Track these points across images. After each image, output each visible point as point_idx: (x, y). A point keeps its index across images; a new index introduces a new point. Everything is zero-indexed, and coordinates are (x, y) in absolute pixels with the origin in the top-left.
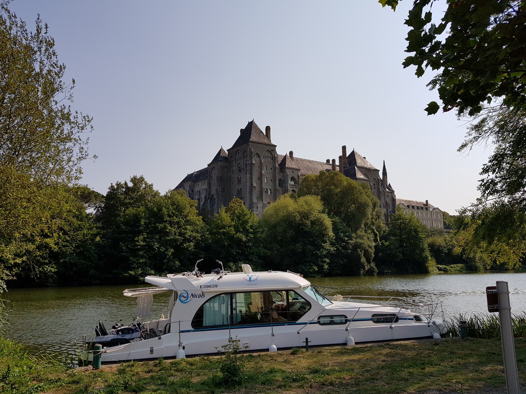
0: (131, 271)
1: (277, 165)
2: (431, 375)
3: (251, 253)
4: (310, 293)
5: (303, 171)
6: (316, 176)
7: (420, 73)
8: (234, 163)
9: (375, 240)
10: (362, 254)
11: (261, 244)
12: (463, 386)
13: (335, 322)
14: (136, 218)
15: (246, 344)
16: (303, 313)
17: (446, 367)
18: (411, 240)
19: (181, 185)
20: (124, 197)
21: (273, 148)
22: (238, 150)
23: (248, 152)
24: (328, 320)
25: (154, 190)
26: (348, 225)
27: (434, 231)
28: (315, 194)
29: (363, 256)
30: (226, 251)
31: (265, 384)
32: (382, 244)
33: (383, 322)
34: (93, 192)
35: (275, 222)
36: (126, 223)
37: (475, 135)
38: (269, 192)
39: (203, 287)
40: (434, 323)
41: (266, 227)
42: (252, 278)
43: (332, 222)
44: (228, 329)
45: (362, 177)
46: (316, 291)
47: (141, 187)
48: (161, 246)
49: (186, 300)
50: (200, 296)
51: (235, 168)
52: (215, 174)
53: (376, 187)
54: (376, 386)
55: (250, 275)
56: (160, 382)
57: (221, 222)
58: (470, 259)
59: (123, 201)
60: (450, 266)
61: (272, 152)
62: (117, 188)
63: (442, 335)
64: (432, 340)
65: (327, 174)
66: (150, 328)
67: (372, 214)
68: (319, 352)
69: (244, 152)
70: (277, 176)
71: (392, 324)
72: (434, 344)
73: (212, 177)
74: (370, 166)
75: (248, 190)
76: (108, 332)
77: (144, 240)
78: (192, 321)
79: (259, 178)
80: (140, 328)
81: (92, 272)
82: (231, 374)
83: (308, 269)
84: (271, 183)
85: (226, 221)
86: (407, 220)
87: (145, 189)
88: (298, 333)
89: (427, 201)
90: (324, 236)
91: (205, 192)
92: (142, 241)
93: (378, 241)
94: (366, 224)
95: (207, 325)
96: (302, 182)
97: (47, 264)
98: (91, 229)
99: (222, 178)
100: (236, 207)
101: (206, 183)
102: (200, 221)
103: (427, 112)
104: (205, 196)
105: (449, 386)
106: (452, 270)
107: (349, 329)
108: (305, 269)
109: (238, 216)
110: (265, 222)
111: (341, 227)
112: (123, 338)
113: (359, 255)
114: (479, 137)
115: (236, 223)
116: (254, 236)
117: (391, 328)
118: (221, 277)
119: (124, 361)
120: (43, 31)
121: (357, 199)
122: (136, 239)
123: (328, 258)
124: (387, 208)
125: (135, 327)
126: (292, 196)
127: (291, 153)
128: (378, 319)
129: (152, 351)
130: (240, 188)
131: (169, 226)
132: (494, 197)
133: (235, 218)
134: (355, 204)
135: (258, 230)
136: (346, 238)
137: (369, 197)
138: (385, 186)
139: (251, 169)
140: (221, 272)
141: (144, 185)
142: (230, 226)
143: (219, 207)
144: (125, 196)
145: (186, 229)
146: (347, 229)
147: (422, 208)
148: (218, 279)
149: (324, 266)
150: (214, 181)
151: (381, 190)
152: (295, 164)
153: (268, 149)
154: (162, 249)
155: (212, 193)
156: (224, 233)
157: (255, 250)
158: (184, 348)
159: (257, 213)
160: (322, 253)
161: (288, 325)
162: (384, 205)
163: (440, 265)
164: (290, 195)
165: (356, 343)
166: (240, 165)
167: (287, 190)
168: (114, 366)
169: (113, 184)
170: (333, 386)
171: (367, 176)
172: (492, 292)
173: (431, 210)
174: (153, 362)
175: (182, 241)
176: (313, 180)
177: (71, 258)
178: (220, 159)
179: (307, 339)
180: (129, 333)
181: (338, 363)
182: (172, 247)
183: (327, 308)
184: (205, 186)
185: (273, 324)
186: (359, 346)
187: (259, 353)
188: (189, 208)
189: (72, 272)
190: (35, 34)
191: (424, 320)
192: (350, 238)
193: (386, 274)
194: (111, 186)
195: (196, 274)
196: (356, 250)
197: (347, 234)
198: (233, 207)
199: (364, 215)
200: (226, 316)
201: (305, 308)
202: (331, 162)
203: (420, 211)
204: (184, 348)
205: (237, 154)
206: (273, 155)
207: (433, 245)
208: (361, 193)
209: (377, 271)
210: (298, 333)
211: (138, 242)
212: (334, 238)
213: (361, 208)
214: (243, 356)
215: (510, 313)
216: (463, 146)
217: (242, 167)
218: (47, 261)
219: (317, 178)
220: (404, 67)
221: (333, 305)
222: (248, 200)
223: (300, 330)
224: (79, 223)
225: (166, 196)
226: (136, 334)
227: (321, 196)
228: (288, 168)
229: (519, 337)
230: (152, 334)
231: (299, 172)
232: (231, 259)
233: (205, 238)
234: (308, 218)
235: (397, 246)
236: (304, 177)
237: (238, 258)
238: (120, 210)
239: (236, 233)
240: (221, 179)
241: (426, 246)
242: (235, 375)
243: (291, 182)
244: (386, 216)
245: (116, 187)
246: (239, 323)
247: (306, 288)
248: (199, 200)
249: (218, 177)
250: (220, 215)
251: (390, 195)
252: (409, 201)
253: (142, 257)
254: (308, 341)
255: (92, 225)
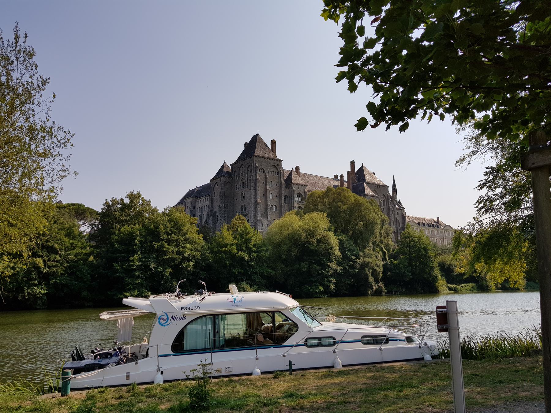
0: (126, 292)
1: (283, 181)
2: (406, 397)
3: (254, 272)
4: (298, 315)
5: (310, 187)
6: (322, 192)
7: (353, 88)
8: (238, 179)
9: (384, 259)
10: (370, 274)
11: (265, 264)
12: (434, 408)
13: (323, 343)
14: (131, 236)
15: (229, 368)
16: (290, 335)
17: (424, 389)
18: (421, 259)
19: (182, 202)
20: (119, 214)
21: (278, 163)
22: (242, 165)
23: (253, 167)
24: (316, 342)
25: (152, 207)
26: (356, 243)
27: (445, 249)
28: (321, 211)
29: (370, 275)
30: (227, 271)
31: (234, 409)
32: (391, 262)
33: (373, 344)
34: (88, 208)
35: (279, 241)
36: (121, 242)
37: (473, 149)
38: (274, 208)
39: (184, 309)
40: (426, 344)
41: (270, 245)
42: (237, 299)
43: (338, 241)
44: (210, 352)
45: (371, 193)
46: (305, 312)
47: (137, 203)
48: (158, 266)
49: (167, 322)
50: (181, 319)
51: (239, 184)
52: (218, 190)
53: (385, 204)
54: (347, 410)
55: (235, 296)
56: (126, 408)
57: (222, 240)
58: (481, 278)
59: (118, 218)
60: (461, 285)
61: (277, 167)
62: (113, 205)
63: (433, 357)
64: (422, 362)
65: (334, 190)
66: (131, 353)
67: (380, 233)
68: (302, 376)
69: (248, 167)
70: (283, 192)
71: (381, 346)
72: (422, 366)
73: (215, 193)
74: (379, 182)
75: (252, 207)
76: (86, 357)
77: (140, 260)
78: (172, 345)
79: (263, 194)
80: (121, 353)
81: (85, 293)
82: (199, 399)
83: (313, 289)
84: (276, 200)
85: (228, 240)
86: (417, 237)
87: (142, 205)
88: (284, 356)
89: (438, 218)
90: (330, 254)
91: (207, 209)
92: (137, 260)
93: (386, 260)
94: (374, 243)
95: (188, 349)
96: (308, 199)
97: (36, 285)
98: (85, 248)
99: (225, 194)
100: (239, 225)
101: (209, 200)
102: (200, 240)
103: (356, 128)
104: (208, 212)
105: (420, 408)
106: (463, 289)
107: (336, 351)
108: (311, 289)
109: (240, 234)
110: (269, 240)
111: (348, 246)
112: (99, 363)
113: (367, 274)
114: (477, 152)
115: (238, 241)
116: (258, 255)
117: (380, 350)
118: (203, 298)
119: (96, 388)
120: (21, 40)
121: (365, 217)
122: (131, 258)
123: (334, 278)
124: (397, 225)
125: (115, 352)
126: (297, 213)
127: (297, 168)
128: (368, 340)
129: (128, 377)
130: (244, 205)
131: (167, 244)
132: (490, 215)
133: (238, 236)
134: (363, 221)
135: (261, 248)
136: (353, 257)
137: (378, 214)
138: (395, 202)
139: (256, 185)
140: (204, 293)
141: (141, 202)
142: (232, 245)
143: (221, 224)
144: (120, 213)
145: (184, 247)
146: (355, 248)
147: (433, 225)
148: (200, 301)
149: (330, 286)
150: (217, 197)
151: (391, 207)
152: (301, 180)
153: (273, 164)
154: (160, 269)
155: (215, 210)
156: (225, 252)
157: (258, 269)
158: (162, 373)
159: (262, 231)
160: (328, 273)
161: (274, 348)
162: (393, 222)
163: (451, 284)
164: (295, 212)
165: (344, 366)
166: (244, 181)
167: (293, 206)
168: (85, 392)
169: (107, 200)
170: (303, 410)
171: (376, 192)
172: (442, 311)
173: (442, 227)
174: (126, 388)
175: (181, 260)
176: (319, 197)
177: (62, 278)
178: (223, 174)
179: (290, 362)
180: (107, 358)
181: (317, 386)
182: (170, 267)
183: (314, 329)
184: (208, 203)
185: (257, 346)
186: (345, 369)
187: (240, 378)
188: (189, 225)
189: (62, 294)
190: (13, 42)
191: (417, 341)
192: (357, 256)
193: (395, 294)
194: (106, 203)
195: (177, 296)
196: (364, 269)
197: (355, 252)
198: (235, 225)
199: (373, 233)
200: (209, 339)
201: (292, 330)
202: (339, 178)
203: (431, 229)
204: (162, 373)
205: (241, 169)
206: (279, 170)
207: (443, 264)
208: (369, 210)
209: (386, 291)
210: (284, 356)
211: (134, 262)
212: (341, 257)
213: (369, 226)
214: (223, 381)
215: (459, 333)
216: (462, 160)
217: (246, 183)
218: (36, 282)
219: (323, 194)
220: (337, 82)
221: (322, 326)
222: (252, 217)
223: (285, 353)
224: (71, 241)
225: (164, 213)
226: (115, 359)
227: (328, 214)
228: (295, 184)
229: (509, 358)
230: (134, 358)
231: (306, 188)
232: (233, 279)
233: (205, 257)
234: (314, 235)
235: (406, 265)
236: (310, 193)
237: (240, 278)
238: (115, 228)
239: (238, 252)
240: (224, 195)
241: (436, 265)
242: (202, 400)
243: (298, 198)
244: (396, 234)
245: (111, 203)
246: (222, 346)
247: (295, 308)
248: (201, 217)
249: (220, 193)
250: (221, 233)
251: (400, 212)
252: (420, 218)
253: (138, 277)
254: (292, 364)
255: (85, 244)
